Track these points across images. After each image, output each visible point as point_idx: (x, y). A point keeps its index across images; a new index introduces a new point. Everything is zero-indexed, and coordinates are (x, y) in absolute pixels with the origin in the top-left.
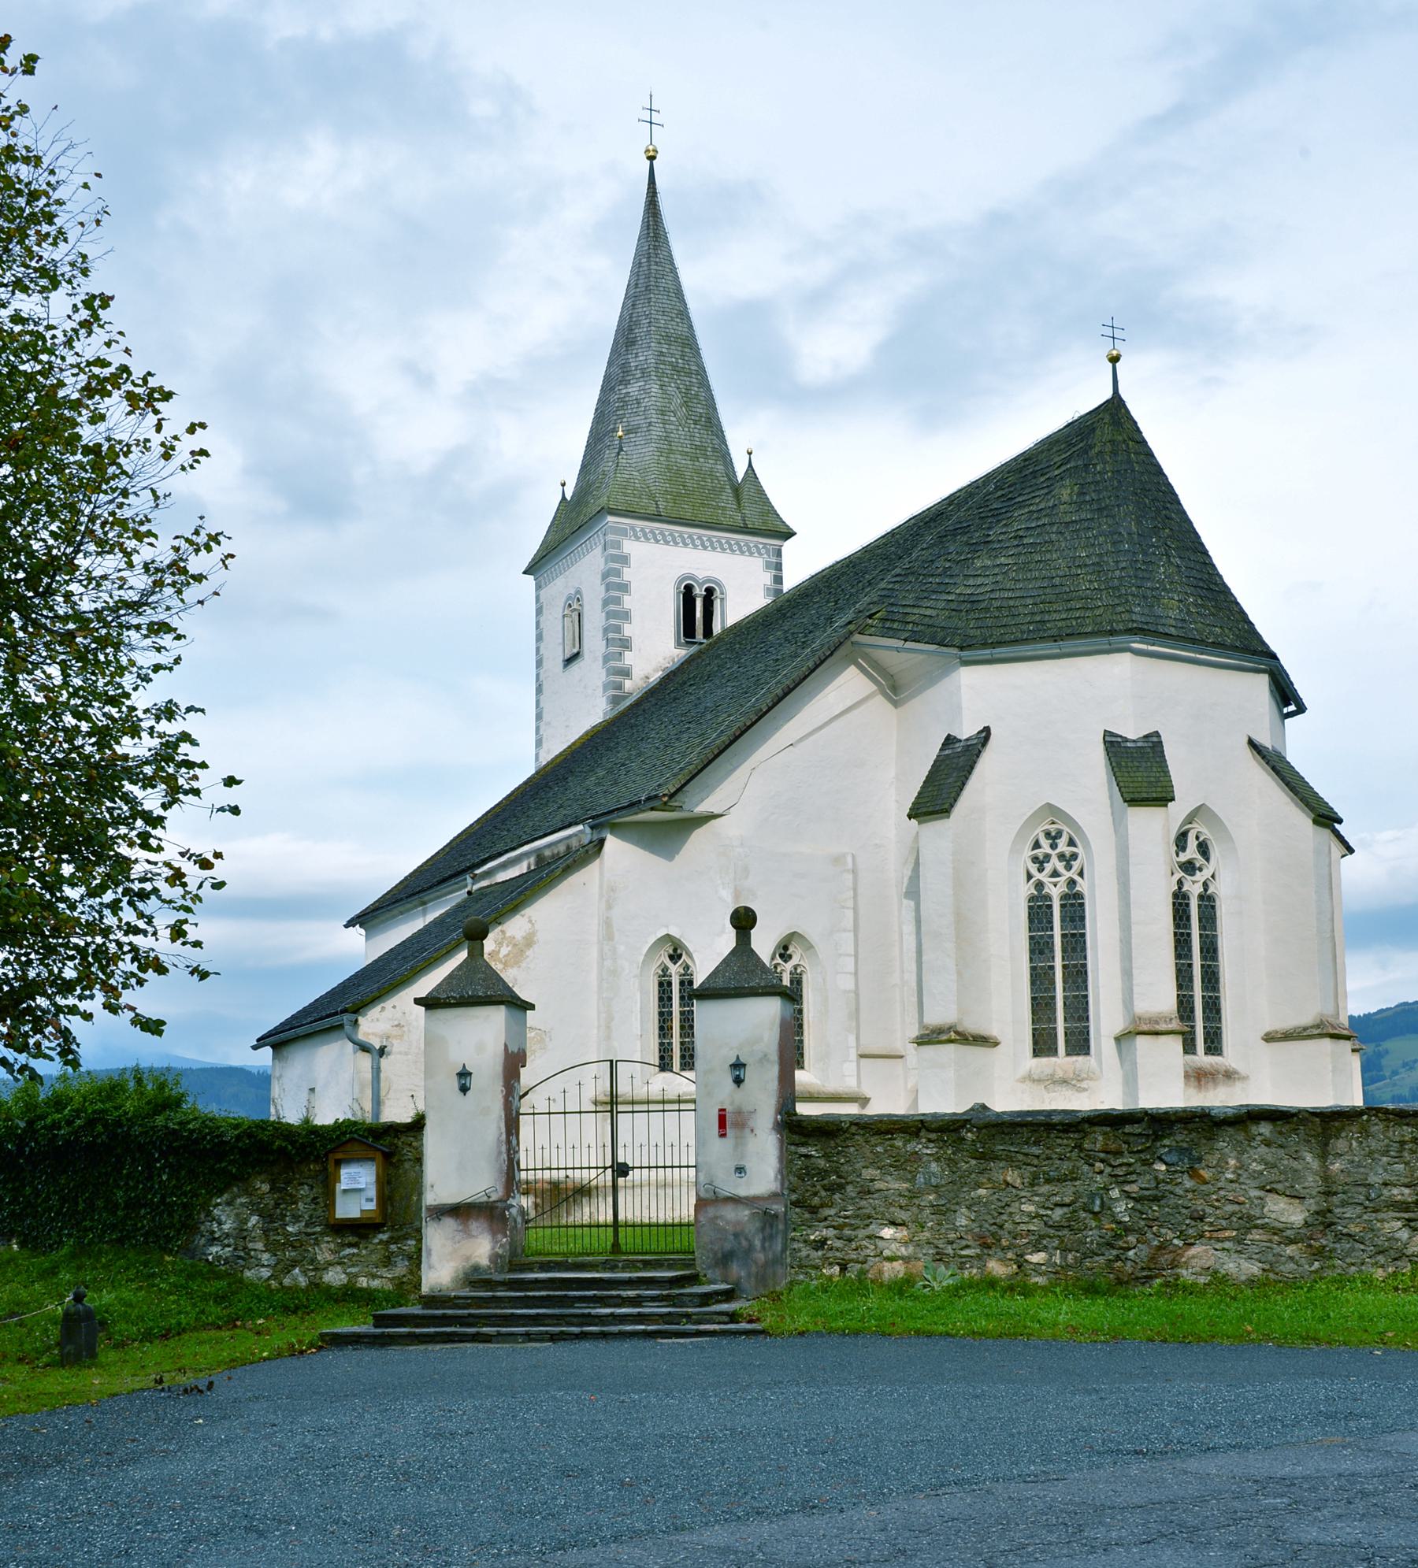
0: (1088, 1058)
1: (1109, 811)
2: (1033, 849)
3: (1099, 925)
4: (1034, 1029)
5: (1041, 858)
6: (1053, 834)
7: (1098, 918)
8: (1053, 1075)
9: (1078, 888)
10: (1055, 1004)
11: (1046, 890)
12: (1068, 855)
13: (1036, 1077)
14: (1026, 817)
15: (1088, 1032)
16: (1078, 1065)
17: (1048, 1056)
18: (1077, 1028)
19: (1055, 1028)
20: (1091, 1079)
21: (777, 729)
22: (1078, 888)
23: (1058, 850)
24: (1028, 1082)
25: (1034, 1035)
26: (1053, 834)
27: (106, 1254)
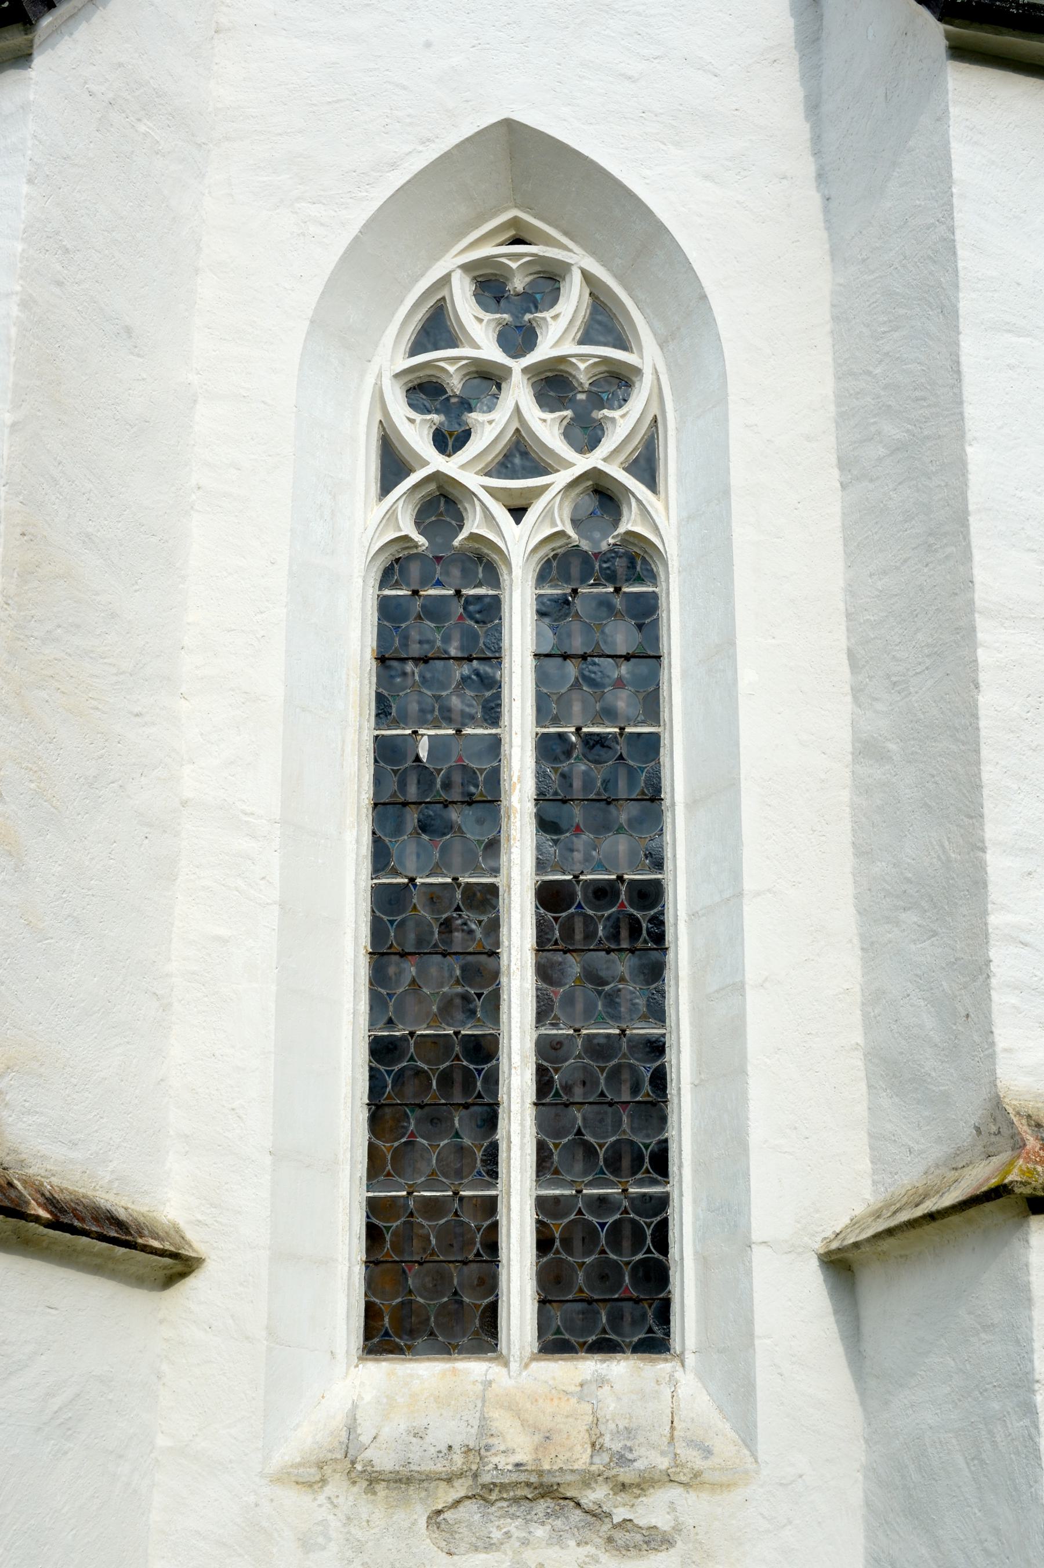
0: (657, 1368)
1: (808, 167)
2: (416, 349)
3: (747, 676)
4: (374, 1206)
5: (455, 384)
6: (518, 284)
7: (745, 641)
8: (476, 1452)
9: (631, 523)
10: (492, 1080)
11: (474, 525)
12: (583, 373)
13: (385, 1461)
14: (398, 179)
15: (662, 1232)
16: (610, 1406)
17: (448, 1350)
18: (602, 1203)
19: (490, 1206)
20: (694, 1481)
21: (31, 1260)
22: (631, 523)
23: (544, 351)
24: (337, 1487)
25: (373, 1235)
26: (518, 284)
27: (491, 1532)
